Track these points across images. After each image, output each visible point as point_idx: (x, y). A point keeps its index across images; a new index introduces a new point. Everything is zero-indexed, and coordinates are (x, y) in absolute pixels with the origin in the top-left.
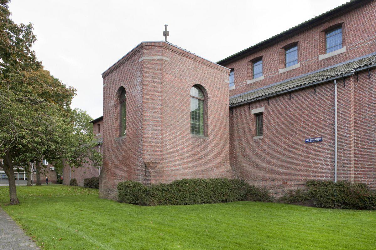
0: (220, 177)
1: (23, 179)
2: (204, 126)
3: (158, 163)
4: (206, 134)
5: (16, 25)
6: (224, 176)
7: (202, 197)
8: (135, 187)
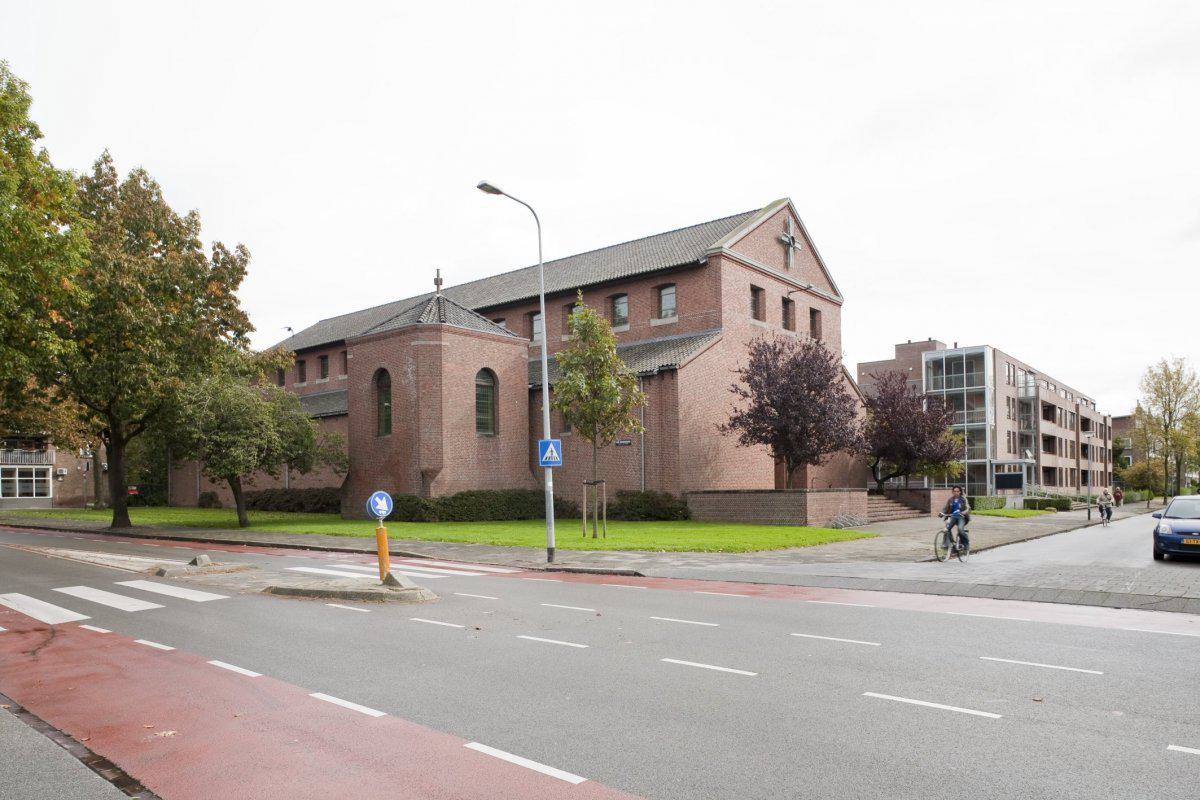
0: (516, 487)
1: (32, 495)
2: (494, 420)
3: (438, 472)
4: (496, 431)
5: (35, 132)
6: (522, 486)
7: (492, 513)
8: (408, 501)
